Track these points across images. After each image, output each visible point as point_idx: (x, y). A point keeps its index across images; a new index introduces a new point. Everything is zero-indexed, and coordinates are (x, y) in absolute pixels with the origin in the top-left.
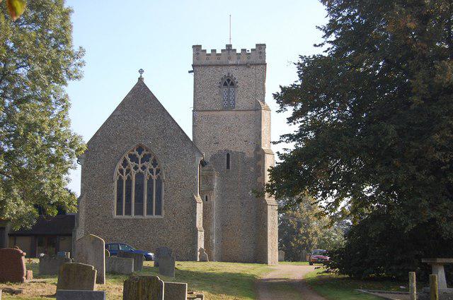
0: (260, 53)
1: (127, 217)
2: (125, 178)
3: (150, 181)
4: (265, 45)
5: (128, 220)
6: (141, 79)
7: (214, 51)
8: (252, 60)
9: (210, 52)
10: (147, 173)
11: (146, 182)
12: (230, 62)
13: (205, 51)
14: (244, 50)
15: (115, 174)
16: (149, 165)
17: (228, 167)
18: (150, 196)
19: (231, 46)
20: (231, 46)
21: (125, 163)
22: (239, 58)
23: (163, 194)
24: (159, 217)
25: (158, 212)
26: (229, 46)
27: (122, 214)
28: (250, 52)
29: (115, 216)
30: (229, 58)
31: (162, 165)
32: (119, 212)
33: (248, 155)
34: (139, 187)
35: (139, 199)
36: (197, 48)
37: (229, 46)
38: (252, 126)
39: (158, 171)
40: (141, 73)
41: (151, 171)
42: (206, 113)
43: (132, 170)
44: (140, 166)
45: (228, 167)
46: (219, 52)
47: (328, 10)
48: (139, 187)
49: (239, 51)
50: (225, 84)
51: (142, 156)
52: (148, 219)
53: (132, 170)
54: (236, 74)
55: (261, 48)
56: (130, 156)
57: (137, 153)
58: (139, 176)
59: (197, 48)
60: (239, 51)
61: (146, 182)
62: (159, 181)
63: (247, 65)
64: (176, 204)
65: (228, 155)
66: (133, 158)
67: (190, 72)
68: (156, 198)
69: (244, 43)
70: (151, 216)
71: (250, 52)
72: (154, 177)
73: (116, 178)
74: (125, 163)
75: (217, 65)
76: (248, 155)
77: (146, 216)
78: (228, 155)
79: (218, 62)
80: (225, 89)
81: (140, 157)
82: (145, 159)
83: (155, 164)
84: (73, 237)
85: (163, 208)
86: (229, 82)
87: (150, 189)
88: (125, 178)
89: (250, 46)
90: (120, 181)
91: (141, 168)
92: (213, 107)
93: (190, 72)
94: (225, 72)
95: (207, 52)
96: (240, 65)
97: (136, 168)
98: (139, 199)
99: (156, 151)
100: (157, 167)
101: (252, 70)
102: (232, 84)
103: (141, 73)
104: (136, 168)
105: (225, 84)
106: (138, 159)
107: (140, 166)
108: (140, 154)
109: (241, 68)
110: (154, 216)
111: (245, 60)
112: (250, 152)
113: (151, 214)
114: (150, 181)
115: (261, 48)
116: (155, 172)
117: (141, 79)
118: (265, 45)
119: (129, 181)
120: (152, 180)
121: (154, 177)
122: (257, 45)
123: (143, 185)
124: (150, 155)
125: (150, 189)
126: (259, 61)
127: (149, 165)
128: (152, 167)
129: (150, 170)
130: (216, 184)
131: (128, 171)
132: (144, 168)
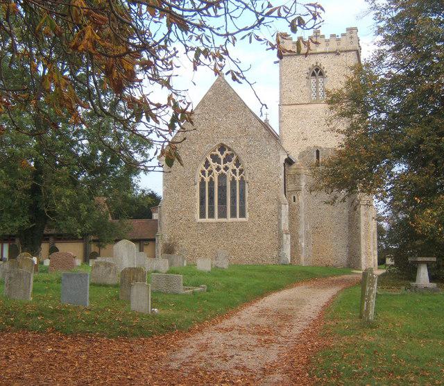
0: (351, 37)
1: (211, 220)
2: (207, 179)
3: (233, 182)
4: (356, 29)
5: (212, 223)
8: (343, 46)
10: (229, 174)
11: (229, 184)
13: (323, 36)
14: (333, 36)
16: (231, 165)
18: (233, 198)
21: (207, 164)
23: (247, 195)
25: (243, 215)
27: (204, 217)
31: (246, 164)
32: (202, 215)
34: (222, 189)
35: (222, 201)
39: (241, 171)
41: (234, 171)
42: (294, 107)
43: (215, 171)
44: (222, 166)
48: (222, 189)
50: (313, 74)
51: (224, 156)
53: (215, 171)
56: (212, 156)
57: (218, 153)
58: (222, 177)
61: (229, 184)
62: (242, 182)
64: (259, 206)
65: (318, 152)
66: (215, 158)
67: (276, 63)
68: (240, 200)
70: (234, 219)
72: (238, 178)
73: (198, 180)
74: (207, 164)
78: (318, 152)
80: (313, 80)
81: (222, 157)
82: (228, 159)
83: (237, 164)
85: (247, 211)
87: (233, 191)
88: (207, 179)
90: (203, 183)
91: (224, 169)
93: (276, 63)
95: (326, 38)
98: (222, 201)
99: (238, 150)
100: (209, 168)
102: (321, 74)
104: (218, 169)
106: (220, 159)
107: (222, 166)
108: (222, 154)
109: (330, 56)
110: (238, 219)
111: (333, 46)
113: (225, 216)
114: (233, 182)
116: (238, 174)
119: (211, 183)
121: (238, 178)
122: (348, 29)
124: (232, 155)
125: (233, 191)
127: (231, 165)
128: (235, 167)
131: (210, 172)
132: (226, 169)
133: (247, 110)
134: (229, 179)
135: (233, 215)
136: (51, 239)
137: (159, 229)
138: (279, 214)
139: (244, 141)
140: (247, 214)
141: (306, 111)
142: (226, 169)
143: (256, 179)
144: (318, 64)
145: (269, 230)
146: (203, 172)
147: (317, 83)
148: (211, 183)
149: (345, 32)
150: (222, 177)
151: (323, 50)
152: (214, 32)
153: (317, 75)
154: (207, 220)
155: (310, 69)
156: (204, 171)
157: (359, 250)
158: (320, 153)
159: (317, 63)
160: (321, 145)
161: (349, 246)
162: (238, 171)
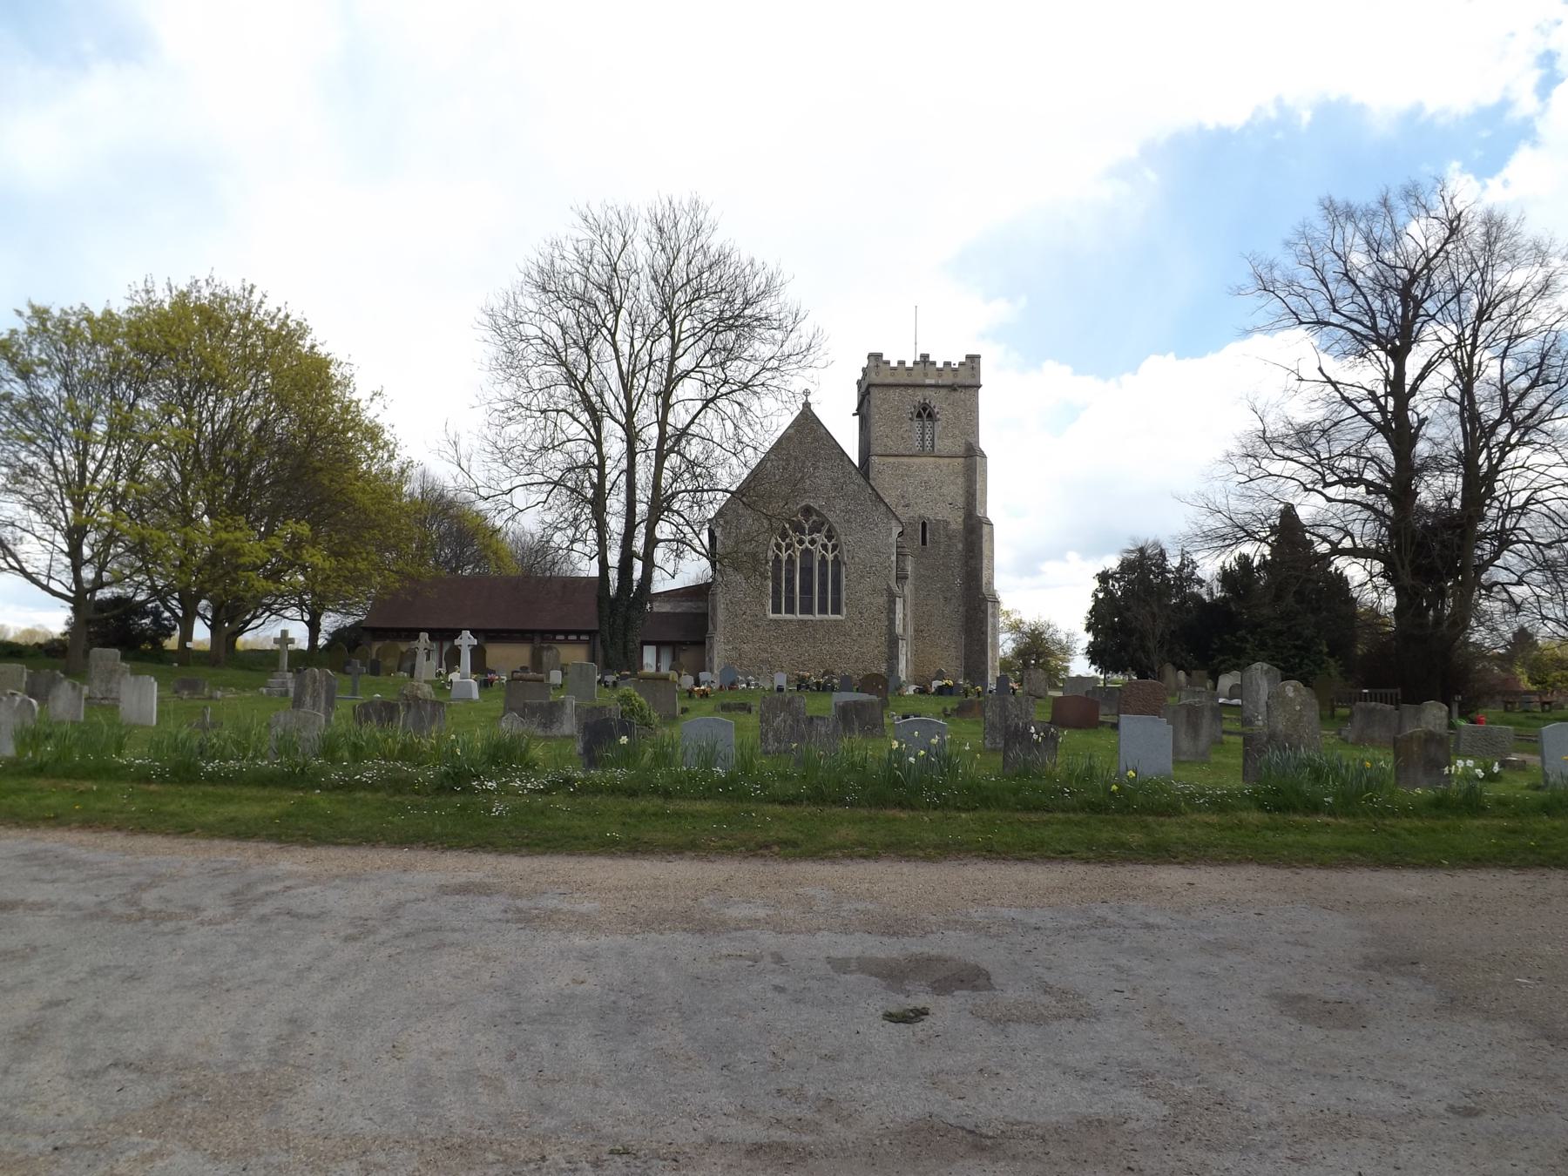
1: (789, 616)
2: (784, 556)
3: (823, 561)
4: (979, 357)
5: (791, 621)
6: (807, 405)
7: (902, 363)
8: (960, 380)
9: (896, 365)
12: (928, 381)
13: (888, 363)
14: (947, 364)
15: (770, 553)
16: (820, 538)
17: (924, 542)
19: (928, 356)
20: (928, 356)
22: (955, 376)
23: (844, 582)
24: (838, 617)
25: (837, 610)
26: (925, 357)
27: (780, 612)
28: (957, 366)
29: (772, 616)
30: (926, 375)
31: (843, 538)
32: (776, 610)
33: (953, 526)
34: (807, 571)
35: (807, 589)
36: (875, 358)
37: (925, 357)
38: (960, 481)
39: (835, 547)
40: (807, 396)
41: (825, 547)
42: (891, 460)
45: (924, 542)
46: (909, 364)
47: (246, 317)
48: (807, 571)
49: (894, 364)
50: (919, 415)
52: (835, 621)
54: (936, 400)
55: (973, 360)
56: (790, 522)
58: (807, 553)
59: (875, 358)
60: (940, 365)
62: (837, 562)
63: (953, 388)
64: (862, 599)
65: (924, 525)
68: (826, 584)
69: (946, 352)
70: (825, 616)
71: (957, 366)
72: (830, 557)
75: (907, 386)
76: (953, 526)
77: (818, 616)
78: (924, 525)
79: (908, 381)
80: (917, 424)
82: (816, 529)
84: (707, 646)
86: (925, 413)
87: (823, 575)
88: (784, 556)
89: (957, 358)
90: (777, 559)
92: (901, 450)
94: (919, 396)
95: (907, 365)
96: (943, 386)
97: (801, 542)
98: (807, 589)
100: (788, 540)
101: (960, 394)
102: (930, 416)
103: (807, 396)
105: (919, 415)
106: (804, 528)
107: (807, 538)
109: (943, 392)
110: (831, 617)
111: (948, 379)
112: (956, 521)
113: (810, 612)
114: (823, 561)
115: (973, 360)
117: (807, 405)
118: (979, 357)
119: (791, 560)
120: (827, 562)
121: (830, 557)
123: (811, 569)
124: (823, 524)
125: (823, 575)
126: (969, 382)
127: (820, 538)
129: (822, 545)
130: (909, 568)
132: (813, 542)
133: (845, 458)
134: (817, 557)
135: (823, 610)
136: (537, 639)
137: (711, 627)
138: (892, 611)
139: (840, 504)
140: (844, 610)
141: (909, 466)
142: (813, 542)
143: (857, 559)
144: (927, 401)
145: (876, 633)
146: (778, 546)
147: (923, 427)
148: (791, 560)
149: (964, 360)
150: (807, 553)
151: (932, 382)
152: (1331, 296)
153: (925, 416)
154: (784, 616)
155: (915, 407)
156: (826, 545)
157: (985, 663)
158: (928, 526)
159: (925, 400)
160: (930, 515)
161: (967, 657)
162: (830, 545)
